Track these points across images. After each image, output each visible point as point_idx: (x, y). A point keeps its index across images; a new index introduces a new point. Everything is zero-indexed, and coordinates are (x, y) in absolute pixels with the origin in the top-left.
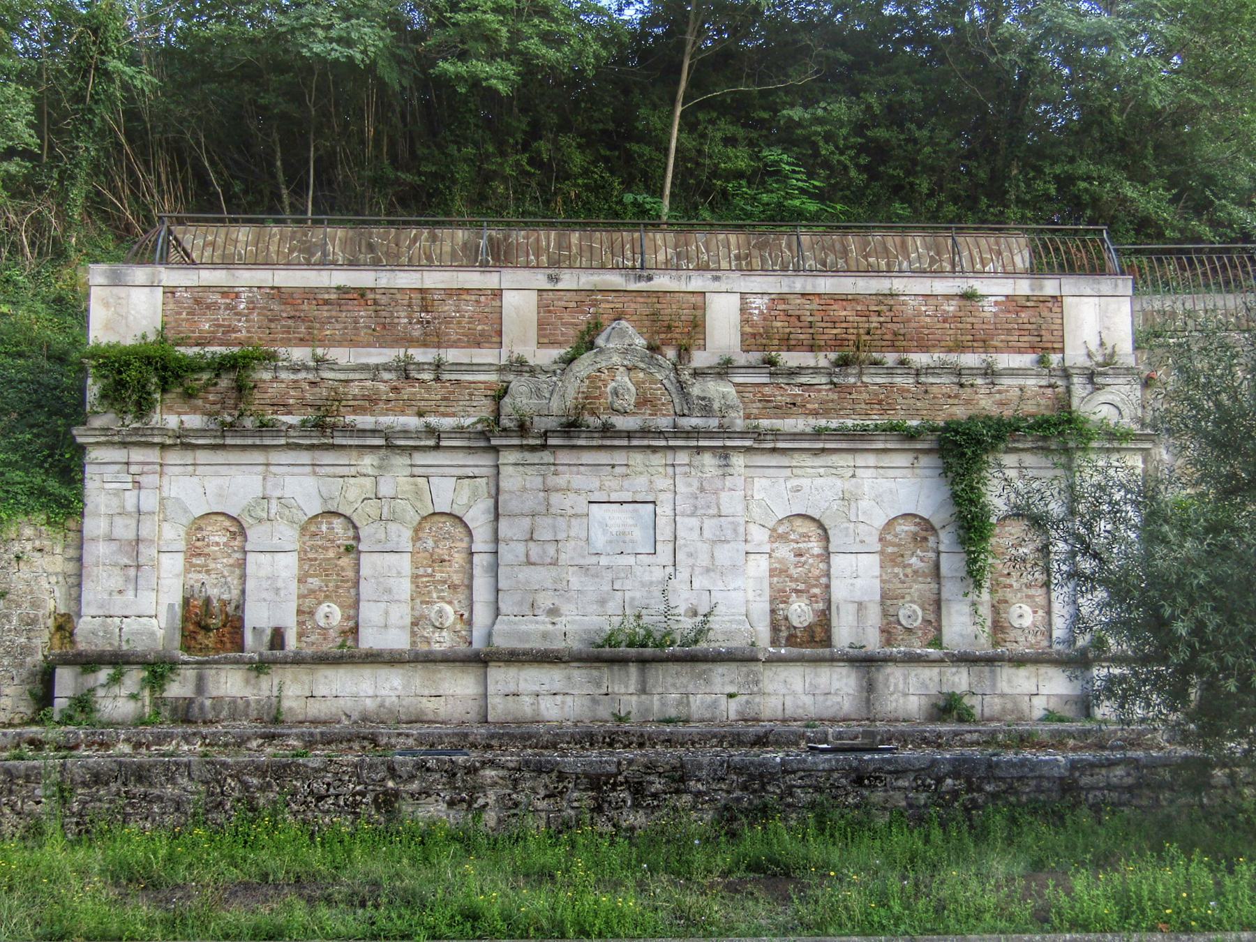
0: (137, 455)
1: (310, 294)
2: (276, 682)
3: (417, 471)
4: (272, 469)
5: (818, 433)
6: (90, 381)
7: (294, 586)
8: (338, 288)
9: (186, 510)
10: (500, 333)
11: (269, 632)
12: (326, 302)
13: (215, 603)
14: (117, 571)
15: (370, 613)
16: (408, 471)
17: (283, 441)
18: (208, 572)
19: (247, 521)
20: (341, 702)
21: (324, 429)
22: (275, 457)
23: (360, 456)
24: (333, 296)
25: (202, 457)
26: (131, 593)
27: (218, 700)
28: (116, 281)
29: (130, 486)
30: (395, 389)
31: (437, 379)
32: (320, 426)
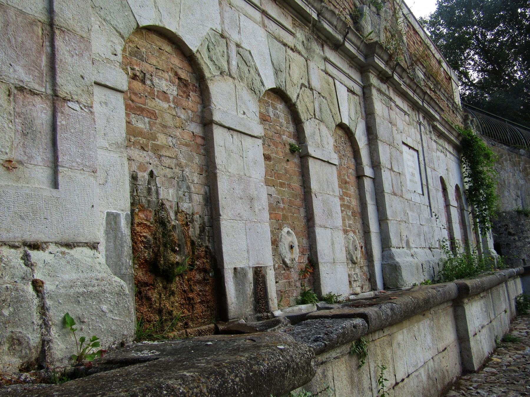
11: (250, 275)
26: (40, 173)
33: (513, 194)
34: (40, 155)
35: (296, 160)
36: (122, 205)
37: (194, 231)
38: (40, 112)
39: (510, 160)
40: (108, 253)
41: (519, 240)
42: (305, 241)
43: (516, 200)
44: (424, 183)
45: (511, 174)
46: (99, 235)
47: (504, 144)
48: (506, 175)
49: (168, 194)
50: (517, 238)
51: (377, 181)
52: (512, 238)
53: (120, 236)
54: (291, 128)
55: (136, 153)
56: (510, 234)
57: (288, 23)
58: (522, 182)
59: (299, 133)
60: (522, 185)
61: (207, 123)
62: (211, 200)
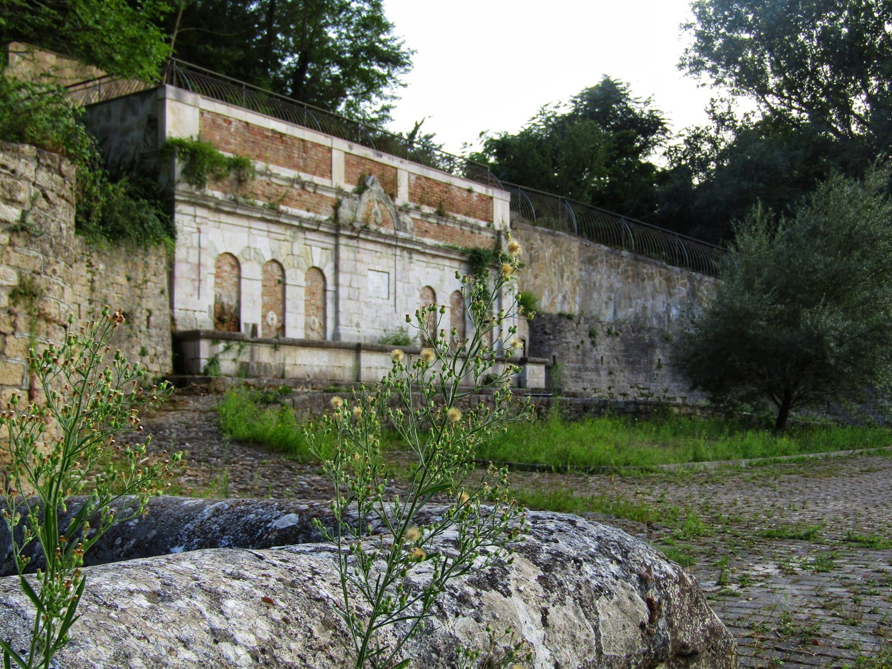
0: (200, 212)
1: (261, 130)
2: (282, 355)
3: (308, 242)
4: (252, 230)
5: (438, 248)
6: (177, 161)
7: (260, 299)
8: (272, 130)
9: (216, 249)
10: (331, 172)
11: (251, 326)
12: (267, 137)
13: (226, 307)
14: (189, 282)
15: (290, 319)
16: (303, 242)
17: (259, 215)
18: (223, 288)
19: (241, 260)
20: (306, 368)
21: (273, 214)
22: (362, 244)
23: (286, 229)
24: (270, 134)
25: (223, 218)
26: (196, 296)
27: (259, 364)
28: (179, 99)
29: (195, 230)
30: (299, 195)
31: (315, 192)
32: (273, 208)
33: (604, 297)
34: (196, 293)
35: (281, 286)
36: (212, 303)
37: (232, 311)
38: (197, 284)
39: (607, 262)
40: (281, 161)
41: (554, 339)
42: (281, 318)
43: (606, 303)
44: (392, 291)
45: (605, 277)
46: (206, 309)
47: (603, 244)
48: (599, 277)
49: (225, 300)
50: (551, 337)
51: (336, 293)
52: (547, 337)
53: (577, 288)
54: (280, 273)
55: (217, 289)
56: (545, 333)
57: (280, 231)
58: (618, 285)
59: (284, 275)
60: (618, 289)
61: (239, 277)
62: (239, 302)
